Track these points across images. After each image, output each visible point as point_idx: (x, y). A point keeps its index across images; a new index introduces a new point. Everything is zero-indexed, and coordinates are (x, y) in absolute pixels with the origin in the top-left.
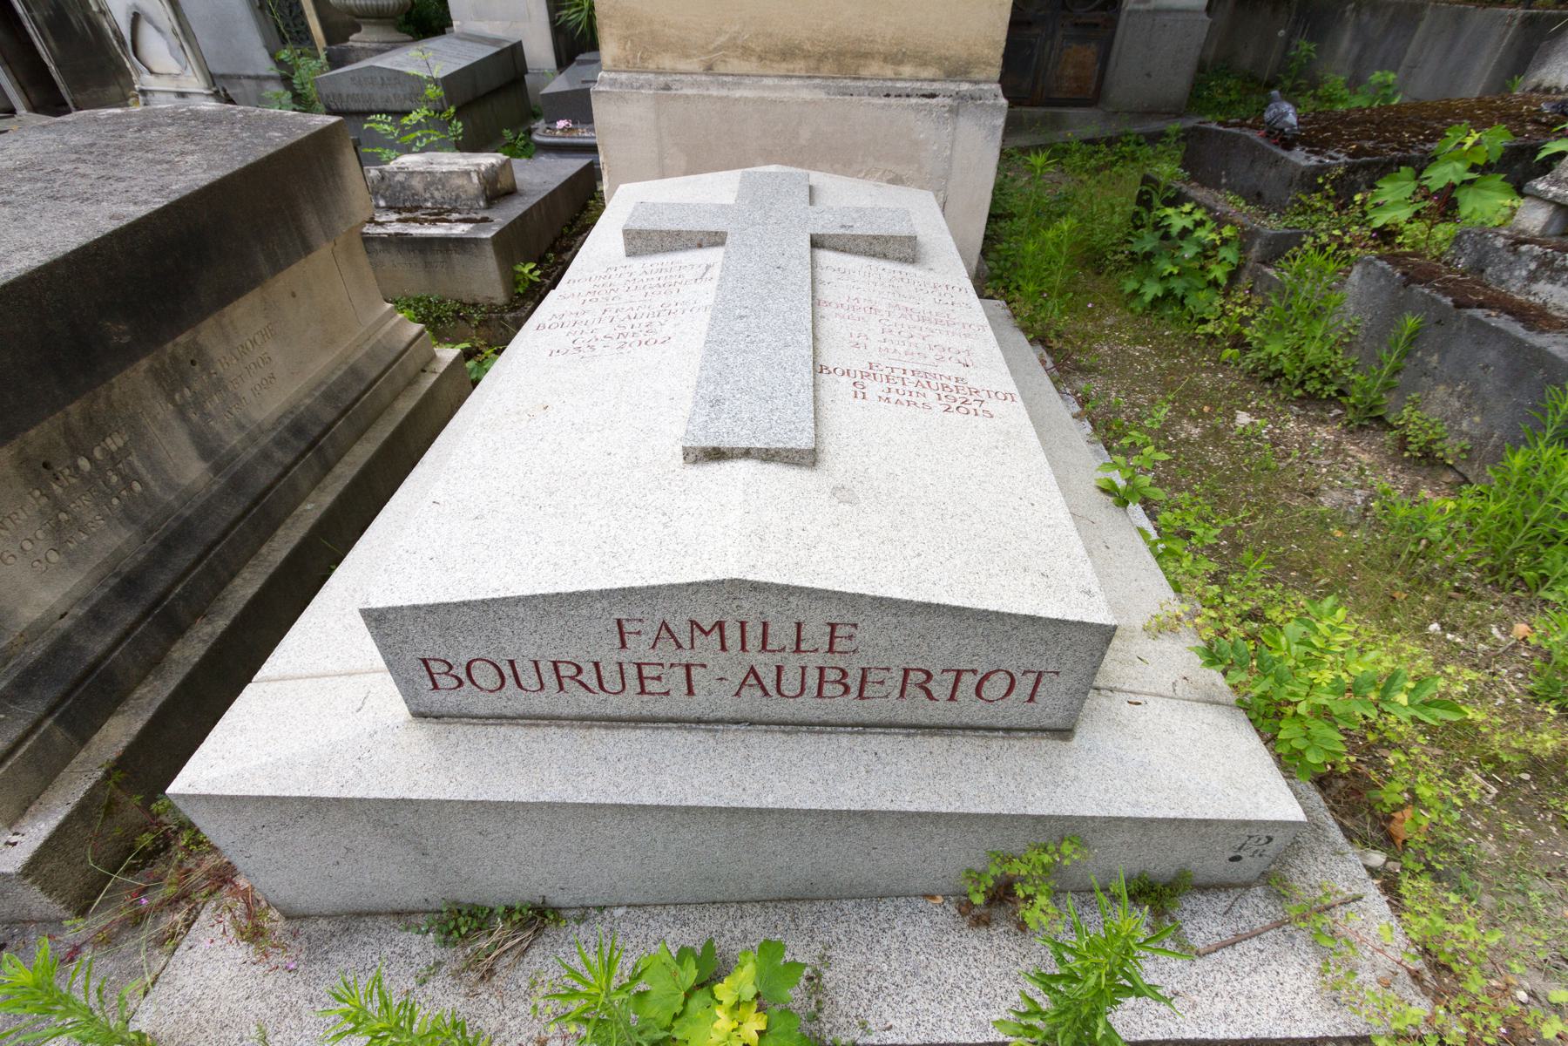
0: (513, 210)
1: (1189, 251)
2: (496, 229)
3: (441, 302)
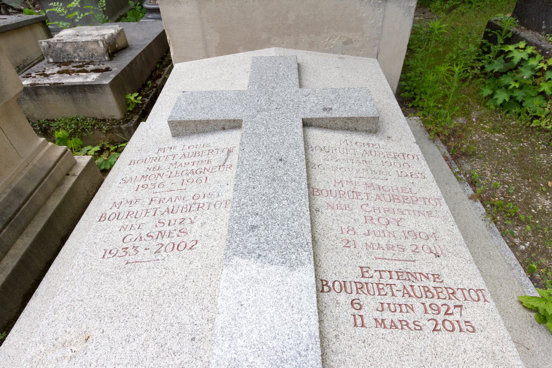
0: (126, 59)
1: (526, 74)
2: (113, 76)
3: (84, 120)
